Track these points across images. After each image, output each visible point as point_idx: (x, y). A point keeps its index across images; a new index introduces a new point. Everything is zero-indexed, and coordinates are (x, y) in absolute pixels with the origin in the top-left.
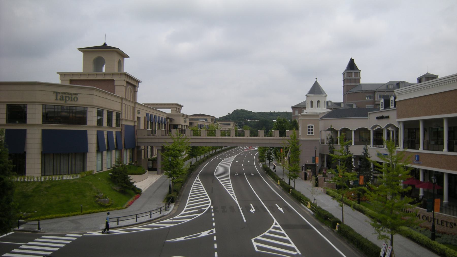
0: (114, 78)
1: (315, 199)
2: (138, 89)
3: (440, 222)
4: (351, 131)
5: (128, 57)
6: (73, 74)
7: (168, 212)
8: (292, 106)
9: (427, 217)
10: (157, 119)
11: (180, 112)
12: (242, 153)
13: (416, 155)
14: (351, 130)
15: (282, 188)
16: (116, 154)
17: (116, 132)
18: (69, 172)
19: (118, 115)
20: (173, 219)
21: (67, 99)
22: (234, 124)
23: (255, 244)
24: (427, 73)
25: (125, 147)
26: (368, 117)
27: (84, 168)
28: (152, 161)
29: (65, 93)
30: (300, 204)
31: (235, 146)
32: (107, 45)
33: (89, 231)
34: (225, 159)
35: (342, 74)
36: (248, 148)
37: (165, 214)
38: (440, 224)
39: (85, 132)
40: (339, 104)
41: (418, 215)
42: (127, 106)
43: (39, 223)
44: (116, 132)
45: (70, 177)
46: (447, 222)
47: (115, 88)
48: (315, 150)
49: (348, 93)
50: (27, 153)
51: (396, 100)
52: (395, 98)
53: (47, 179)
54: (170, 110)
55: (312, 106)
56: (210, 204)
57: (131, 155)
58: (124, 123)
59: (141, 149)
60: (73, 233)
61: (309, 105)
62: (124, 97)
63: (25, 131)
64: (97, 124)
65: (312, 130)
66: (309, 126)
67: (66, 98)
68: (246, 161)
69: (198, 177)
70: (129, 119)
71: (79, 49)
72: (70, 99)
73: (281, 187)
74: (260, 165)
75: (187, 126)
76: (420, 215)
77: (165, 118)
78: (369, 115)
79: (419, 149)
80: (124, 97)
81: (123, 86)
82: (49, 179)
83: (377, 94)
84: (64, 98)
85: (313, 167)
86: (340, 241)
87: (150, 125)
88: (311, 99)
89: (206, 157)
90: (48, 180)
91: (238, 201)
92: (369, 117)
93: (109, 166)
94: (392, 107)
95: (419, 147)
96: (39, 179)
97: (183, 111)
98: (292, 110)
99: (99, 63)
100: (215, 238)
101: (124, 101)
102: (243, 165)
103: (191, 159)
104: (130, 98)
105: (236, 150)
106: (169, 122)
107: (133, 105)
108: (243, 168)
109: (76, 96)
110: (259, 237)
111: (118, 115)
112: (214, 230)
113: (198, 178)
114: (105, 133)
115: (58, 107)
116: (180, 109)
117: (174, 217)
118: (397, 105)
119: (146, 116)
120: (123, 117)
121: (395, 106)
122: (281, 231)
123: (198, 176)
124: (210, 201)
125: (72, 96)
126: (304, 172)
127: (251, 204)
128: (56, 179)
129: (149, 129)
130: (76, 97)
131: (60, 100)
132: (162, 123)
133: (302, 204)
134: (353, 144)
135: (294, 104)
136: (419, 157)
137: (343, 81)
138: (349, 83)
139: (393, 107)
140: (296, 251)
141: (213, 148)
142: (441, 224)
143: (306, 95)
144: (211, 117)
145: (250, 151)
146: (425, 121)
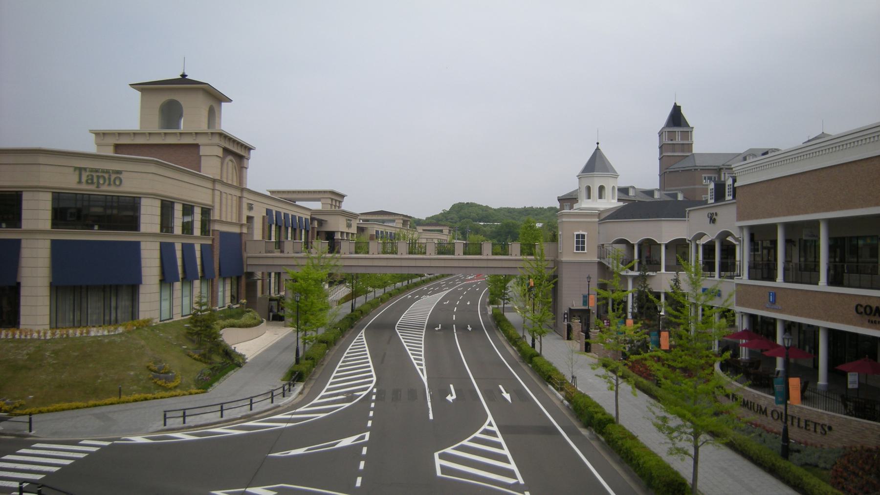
1: (573, 377)
2: (248, 163)
3: (803, 424)
4: (660, 245)
5: (229, 100)
6: (120, 134)
7: (287, 400)
8: (558, 197)
9: (780, 413)
10: (304, 223)
11: (339, 207)
12: (460, 287)
13: (770, 293)
14: (659, 243)
15: (519, 354)
16: (182, 289)
17: (183, 244)
18: (74, 325)
19: (206, 212)
20: (293, 414)
21: (101, 181)
22: (450, 230)
23: (438, 462)
24: (823, 133)
25: (220, 275)
26: (686, 218)
27: (134, 314)
29: (97, 171)
30: (548, 385)
31: (450, 273)
32: (186, 77)
33: (126, 435)
34: (424, 298)
35: (658, 135)
36: (473, 276)
38: (802, 428)
40: (650, 193)
41: (763, 409)
42: (224, 196)
43: (30, 419)
44: (201, 244)
45: (104, 331)
46: (815, 424)
47: (200, 161)
48: (589, 282)
49: (670, 172)
50: (22, 284)
51: (736, 185)
52: (734, 181)
53: (58, 336)
54: (320, 202)
55: (589, 197)
56: (372, 385)
57: (235, 290)
58: (217, 227)
60: (98, 438)
61: (584, 193)
62: (219, 178)
63: (18, 242)
65: (583, 242)
66: (576, 235)
68: (463, 301)
70: (229, 220)
71: (132, 86)
72: (107, 182)
73: (518, 353)
74: (488, 310)
75: (353, 234)
76: (768, 410)
77: (308, 219)
78: (688, 214)
79: (775, 281)
80: (218, 178)
81: (217, 156)
82: (62, 335)
83: (725, 174)
84: (95, 180)
85: (583, 315)
86: (607, 457)
87: (274, 232)
88: (586, 182)
89: (388, 293)
91: (428, 378)
92: (688, 217)
93: (187, 311)
94: (729, 198)
95: (819, 279)
96: (42, 334)
98: (559, 204)
100: (365, 451)
101: (218, 187)
102: (455, 310)
103: (354, 300)
104: (232, 180)
105: (450, 280)
106: (316, 226)
107: (238, 194)
108: (454, 316)
109: (118, 175)
110: (449, 450)
112: (367, 435)
113: (362, 333)
114: (197, 248)
115: (112, 199)
116: (340, 202)
117: (295, 410)
118: (736, 195)
119: (267, 215)
120: (216, 215)
121: (734, 197)
123: (363, 331)
124: (374, 379)
125: (110, 176)
126: (566, 323)
127: (451, 386)
128: (75, 334)
129: (273, 239)
131: (87, 182)
132: (300, 227)
133: (550, 386)
134: (663, 270)
135: (562, 194)
136: (775, 295)
137: (659, 148)
138: (679, 152)
139: (731, 198)
140: (515, 477)
141: (402, 278)
142: (804, 426)
143: (577, 175)
144: (402, 217)
145: (476, 283)
146: (788, 226)
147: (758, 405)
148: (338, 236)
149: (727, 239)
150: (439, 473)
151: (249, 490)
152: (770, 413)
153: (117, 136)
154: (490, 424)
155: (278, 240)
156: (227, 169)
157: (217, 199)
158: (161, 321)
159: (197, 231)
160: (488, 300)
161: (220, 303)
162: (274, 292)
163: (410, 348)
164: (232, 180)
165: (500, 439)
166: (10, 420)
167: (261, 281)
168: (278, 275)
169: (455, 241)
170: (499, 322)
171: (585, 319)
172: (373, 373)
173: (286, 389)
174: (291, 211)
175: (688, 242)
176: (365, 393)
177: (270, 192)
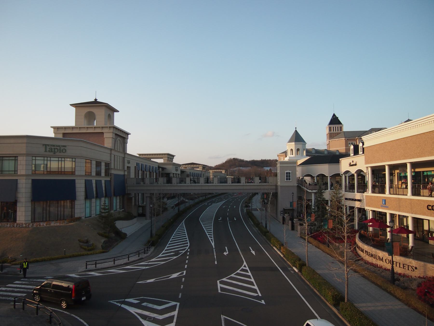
0: (104, 131)
3: (402, 266)
4: (327, 176)
6: (65, 128)
7: (146, 255)
9: (390, 261)
10: (140, 167)
11: (172, 161)
17: (96, 180)
19: (107, 165)
21: (56, 150)
23: (219, 285)
28: (142, 208)
32: (97, 101)
37: (143, 257)
39: (74, 181)
41: (381, 258)
48: (293, 196)
52: (363, 145)
56: (187, 248)
58: (113, 172)
59: (132, 196)
64: (105, 176)
65: (290, 176)
66: (286, 173)
67: (55, 150)
69: (184, 222)
71: (72, 105)
72: (59, 151)
79: (385, 194)
84: (53, 150)
90: (15, 224)
93: (98, 213)
94: (360, 153)
97: (175, 161)
99: (90, 117)
101: (113, 152)
104: (120, 149)
107: (122, 155)
110: (224, 279)
111: (107, 165)
112: (185, 272)
113: (183, 222)
114: (94, 182)
116: (172, 159)
119: (137, 166)
122: (248, 273)
124: (189, 244)
127: (226, 247)
130: (64, 149)
131: (49, 151)
139: (362, 153)
140: (257, 293)
142: (402, 267)
145: (238, 197)
147: (378, 256)
148: (172, 175)
149: (361, 173)
150: (219, 291)
151: (126, 300)
152: (385, 260)
153: (79, 129)
154: (245, 266)
155: (142, 178)
156: (117, 144)
157: (113, 158)
158: (96, 215)
159: (103, 174)
160: (244, 205)
161: (115, 209)
162: (140, 203)
163: (206, 229)
164: (120, 149)
165: (250, 274)
166: (11, 267)
167: (134, 197)
168: (143, 194)
169: (227, 177)
170: (250, 215)
171: (291, 214)
172: (188, 242)
173: (145, 250)
174: (148, 163)
175: (341, 175)
176: (184, 251)
177: (138, 154)
